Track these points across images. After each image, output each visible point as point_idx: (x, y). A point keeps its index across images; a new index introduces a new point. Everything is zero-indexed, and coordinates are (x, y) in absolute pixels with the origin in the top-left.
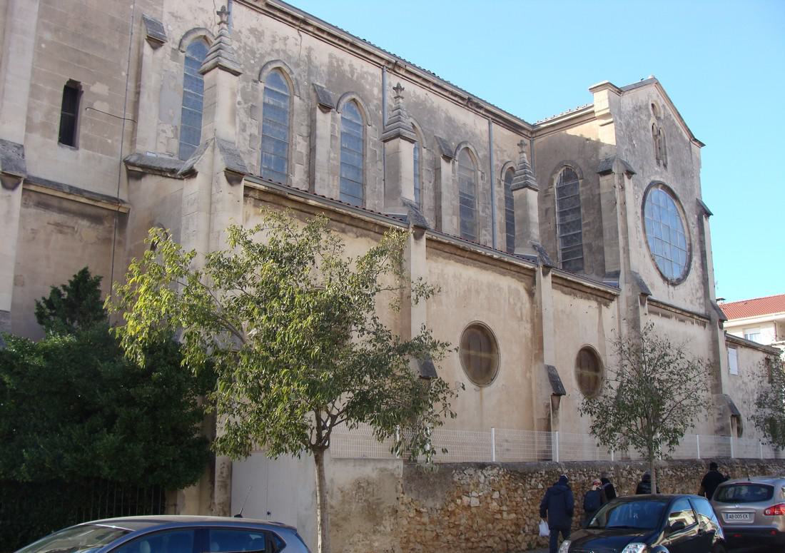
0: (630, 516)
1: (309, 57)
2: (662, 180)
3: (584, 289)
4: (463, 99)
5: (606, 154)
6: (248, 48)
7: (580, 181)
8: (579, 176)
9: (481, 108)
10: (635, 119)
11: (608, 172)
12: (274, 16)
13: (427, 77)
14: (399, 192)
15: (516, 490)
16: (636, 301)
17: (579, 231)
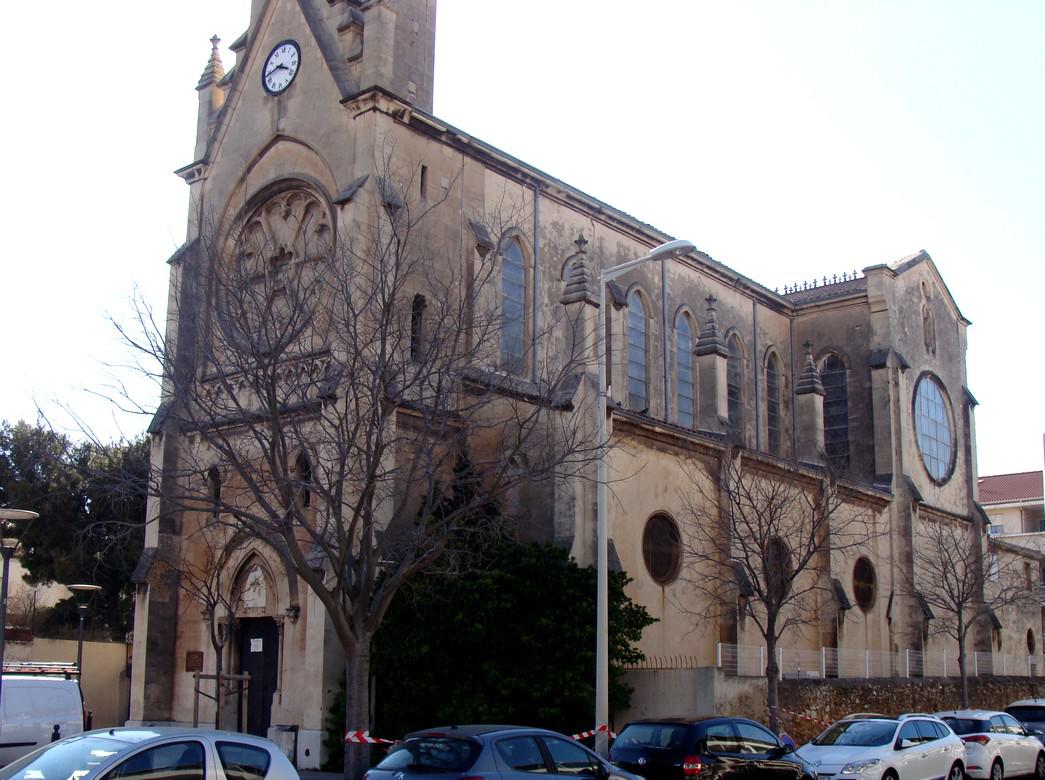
0: (711, 731)
1: (601, 248)
2: (931, 369)
3: (860, 496)
4: (731, 279)
5: (879, 344)
6: (552, 245)
7: (848, 371)
8: (846, 365)
9: (747, 288)
10: (907, 303)
11: (882, 366)
12: (572, 207)
13: (700, 260)
14: (716, 411)
15: (840, 705)
16: (909, 508)
17: (844, 426)
